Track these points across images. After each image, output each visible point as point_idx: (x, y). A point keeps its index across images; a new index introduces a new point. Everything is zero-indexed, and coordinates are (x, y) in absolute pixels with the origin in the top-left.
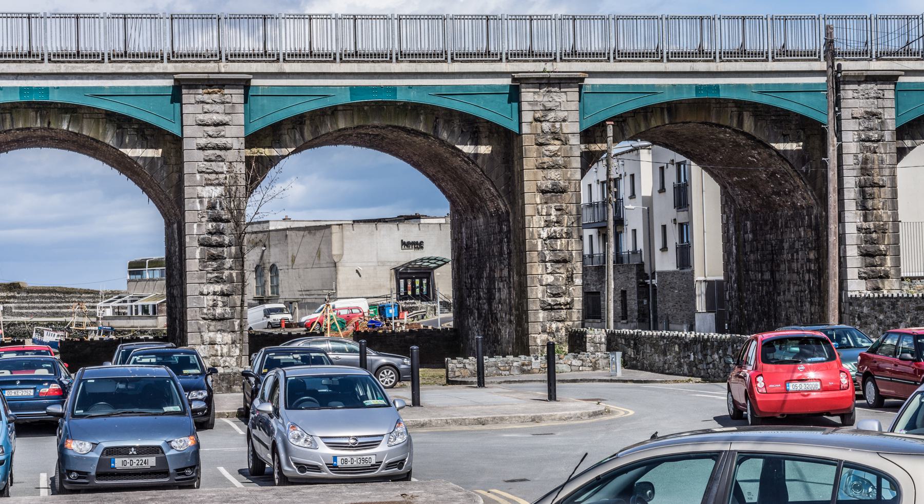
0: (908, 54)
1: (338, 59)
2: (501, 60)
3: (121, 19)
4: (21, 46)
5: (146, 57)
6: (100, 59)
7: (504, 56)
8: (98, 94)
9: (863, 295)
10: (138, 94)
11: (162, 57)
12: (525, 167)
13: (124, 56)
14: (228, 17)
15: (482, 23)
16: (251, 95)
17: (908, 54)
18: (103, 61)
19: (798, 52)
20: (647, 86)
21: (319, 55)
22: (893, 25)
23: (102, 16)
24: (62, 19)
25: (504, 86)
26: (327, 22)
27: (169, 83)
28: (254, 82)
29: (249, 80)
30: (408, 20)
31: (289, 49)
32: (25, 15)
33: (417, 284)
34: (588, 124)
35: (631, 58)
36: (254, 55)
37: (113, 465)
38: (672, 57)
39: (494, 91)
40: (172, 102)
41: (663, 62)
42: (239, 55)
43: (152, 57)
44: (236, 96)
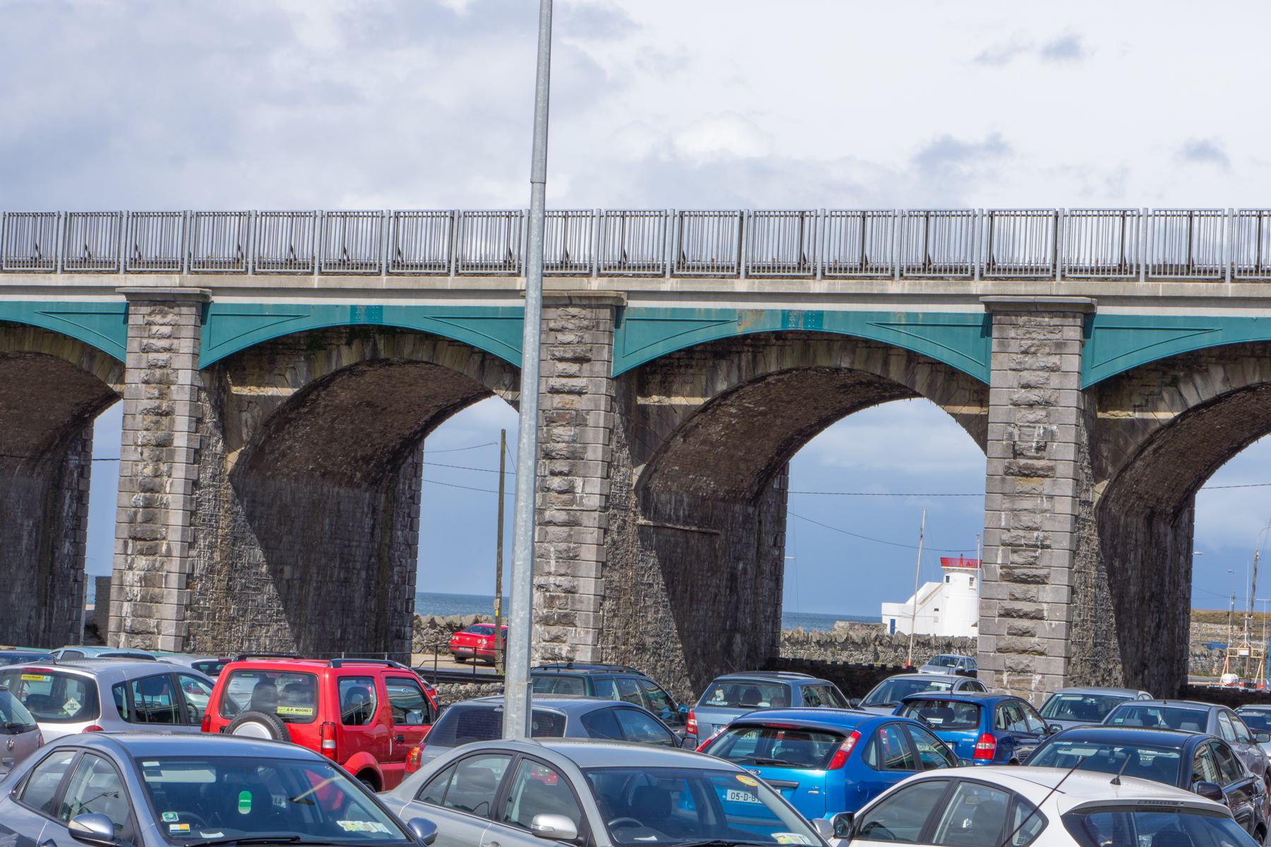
0: (566, 267)
1: (1228, 277)
2: (1223, 279)
3: (1185, 218)
4: (1076, 257)
5: (835, 272)
6: (660, 272)
7: (897, 273)
8: (883, 322)
9: (879, 664)
10: (933, 323)
11: (591, 269)
12: (989, 438)
13: (927, 268)
14: (907, 214)
15: (1114, 223)
16: (1096, 328)
17: (566, 267)
18: (589, 275)
19: (1165, 266)
20: (1185, 318)
21: (1005, 270)
22: (365, 224)
23: (1226, 213)
24: (1101, 218)
25: (975, 315)
26: (1047, 220)
27: (980, 309)
28: (1102, 310)
29: (1091, 306)
30: (1089, 218)
31: (473, 258)
32: (1117, 213)
33: (252, 558)
34: (1095, 377)
35: (1179, 276)
36: (1026, 270)
37: (724, 797)
38: (1154, 273)
39: (957, 323)
40: (982, 336)
41: (449, 275)
42: (1032, 270)
43: (962, 272)
44: (187, 315)
